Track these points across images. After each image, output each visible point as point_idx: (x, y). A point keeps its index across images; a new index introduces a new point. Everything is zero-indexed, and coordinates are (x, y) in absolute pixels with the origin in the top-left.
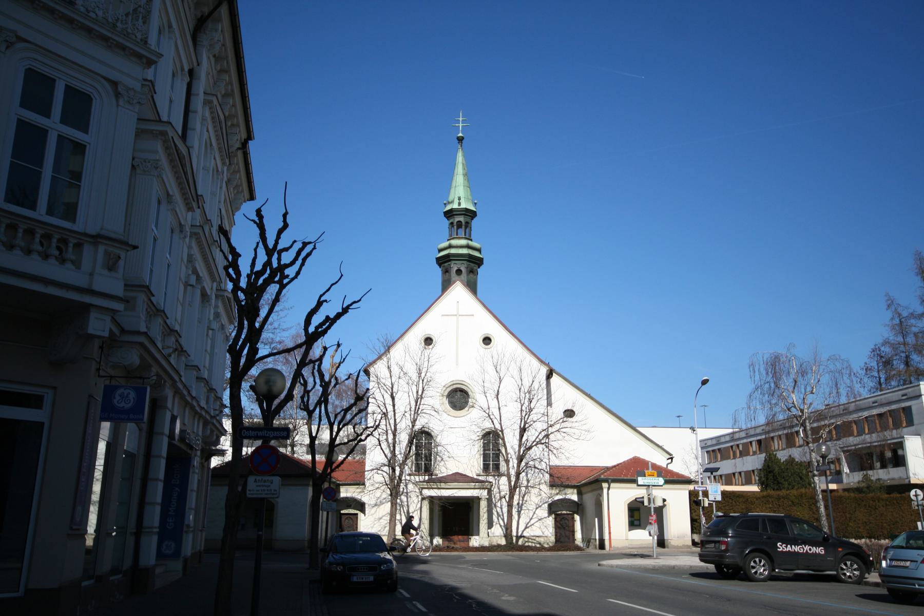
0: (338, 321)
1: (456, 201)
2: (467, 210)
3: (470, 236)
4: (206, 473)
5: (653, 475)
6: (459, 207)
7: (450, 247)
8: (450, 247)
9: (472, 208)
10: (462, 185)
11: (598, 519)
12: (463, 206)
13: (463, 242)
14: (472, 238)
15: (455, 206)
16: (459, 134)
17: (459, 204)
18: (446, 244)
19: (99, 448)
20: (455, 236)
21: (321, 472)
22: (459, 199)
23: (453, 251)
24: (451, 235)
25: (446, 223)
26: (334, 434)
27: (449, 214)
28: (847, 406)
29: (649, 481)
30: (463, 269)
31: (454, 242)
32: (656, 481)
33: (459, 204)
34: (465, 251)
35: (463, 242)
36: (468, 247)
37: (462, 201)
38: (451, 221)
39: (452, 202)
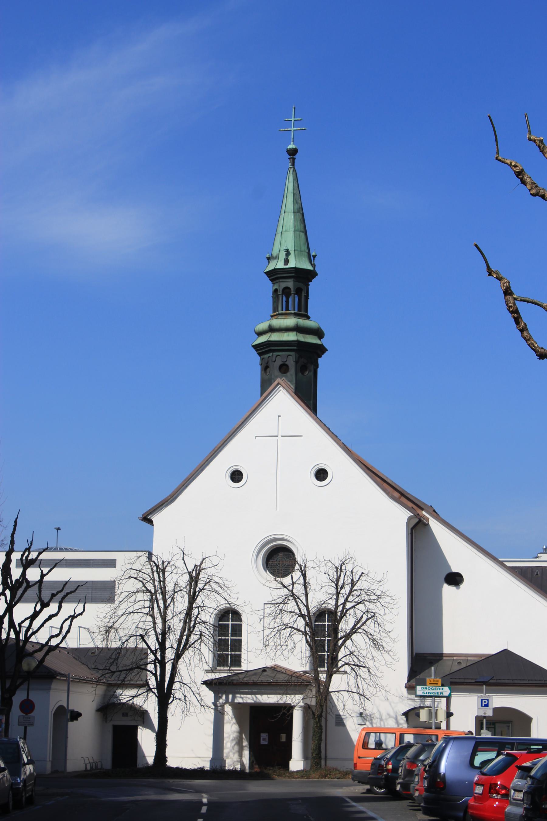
0: (14, 539)
1: (283, 255)
2: (296, 270)
3: (306, 310)
4: (176, 495)
5: (437, 684)
6: (286, 267)
7: (271, 330)
8: (271, 330)
9: (306, 265)
10: (292, 229)
11: (541, 748)
12: (292, 264)
13: (290, 322)
14: (309, 314)
15: (280, 265)
16: (290, 144)
17: (287, 262)
18: (263, 326)
19: (293, 739)
20: (280, 312)
21: (227, 768)
22: (288, 253)
23: (275, 337)
24: (275, 309)
25: (269, 287)
26: (339, 573)
27: (274, 275)
28: (265, 669)
29: (431, 691)
30: (291, 363)
31: (278, 322)
32: (439, 691)
33: (287, 262)
34: (291, 337)
35: (290, 322)
36: (297, 329)
37: (292, 258)
38: (276, 287)
39: (277, 257)
